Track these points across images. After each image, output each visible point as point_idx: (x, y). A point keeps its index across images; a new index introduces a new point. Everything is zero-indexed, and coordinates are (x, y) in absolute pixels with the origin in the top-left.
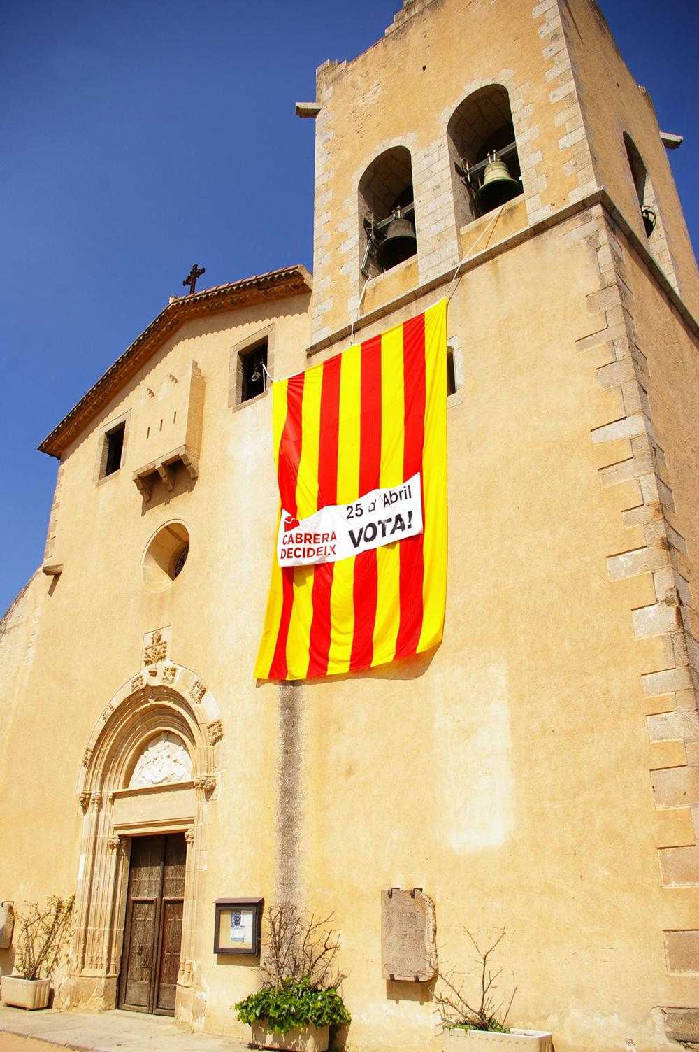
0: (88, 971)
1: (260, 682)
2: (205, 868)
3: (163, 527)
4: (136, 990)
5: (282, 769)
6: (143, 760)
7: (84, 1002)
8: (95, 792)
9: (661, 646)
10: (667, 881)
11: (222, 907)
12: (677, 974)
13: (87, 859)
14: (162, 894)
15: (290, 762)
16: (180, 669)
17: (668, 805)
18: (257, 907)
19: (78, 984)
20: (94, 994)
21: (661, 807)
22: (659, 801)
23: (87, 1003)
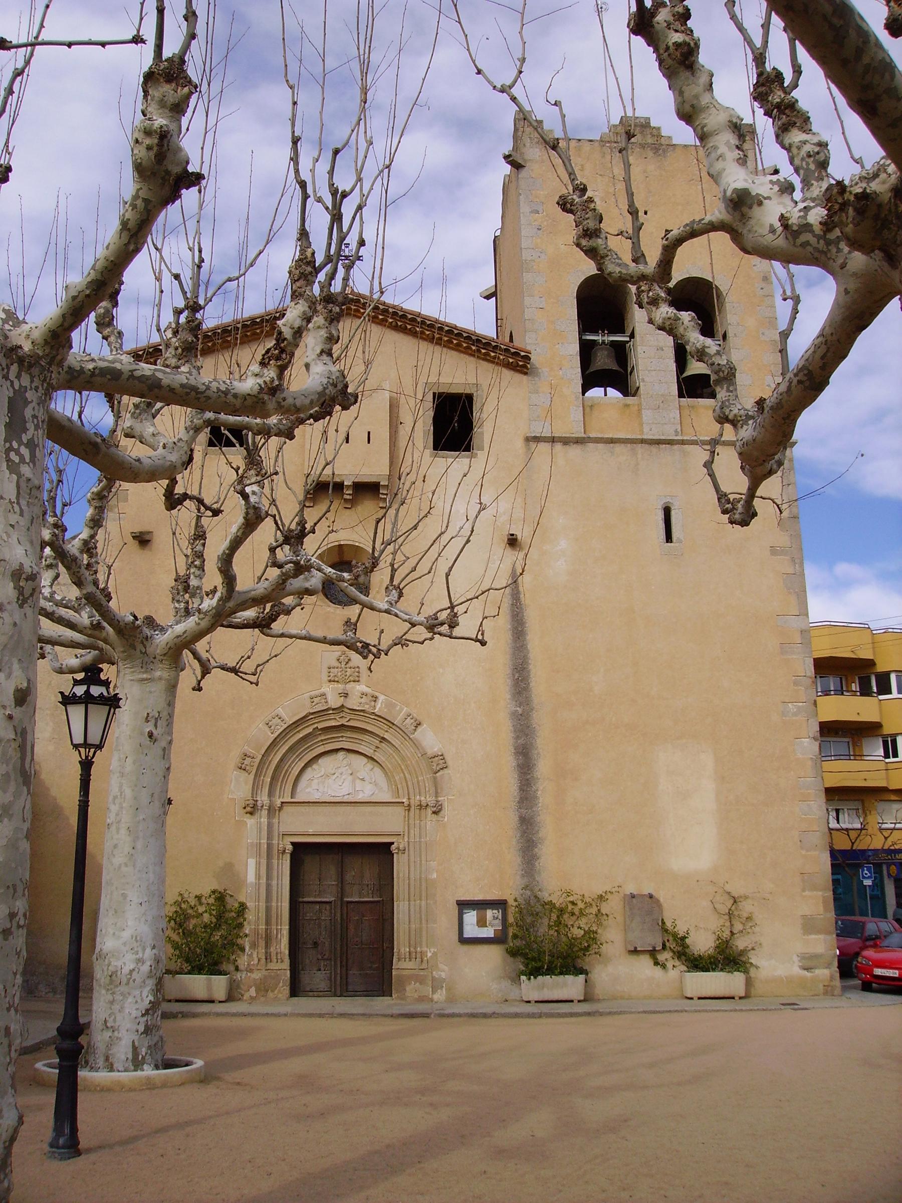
0: (273, 966)
1: (62, 693)
2: (435, 876)
3: (337, 543)
4: (317, 978)
5: (519, 802)
6: (309, 773)
7: (272, 991)
8: (263, 798)
9: (810, 763)
10: (804, 890)
11: (463, 905)
12: (806, 937)
13: (258, 864)
14: (342, 893)
15: (527, 799)
16: (382, 698)
17: (807, 851)
18: (500, 904)
19: (265, 977)
20: (281, 984)
21: (804, 852)
22: (802, 848)
23: (276, 992)
